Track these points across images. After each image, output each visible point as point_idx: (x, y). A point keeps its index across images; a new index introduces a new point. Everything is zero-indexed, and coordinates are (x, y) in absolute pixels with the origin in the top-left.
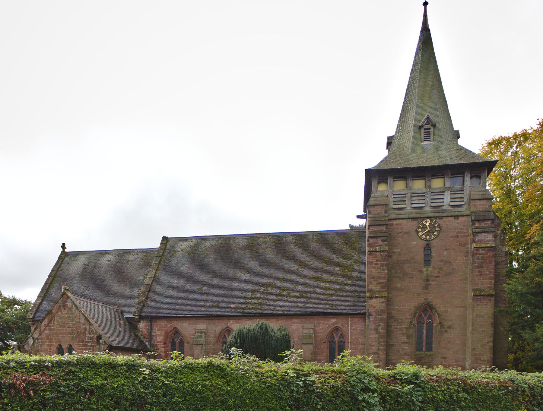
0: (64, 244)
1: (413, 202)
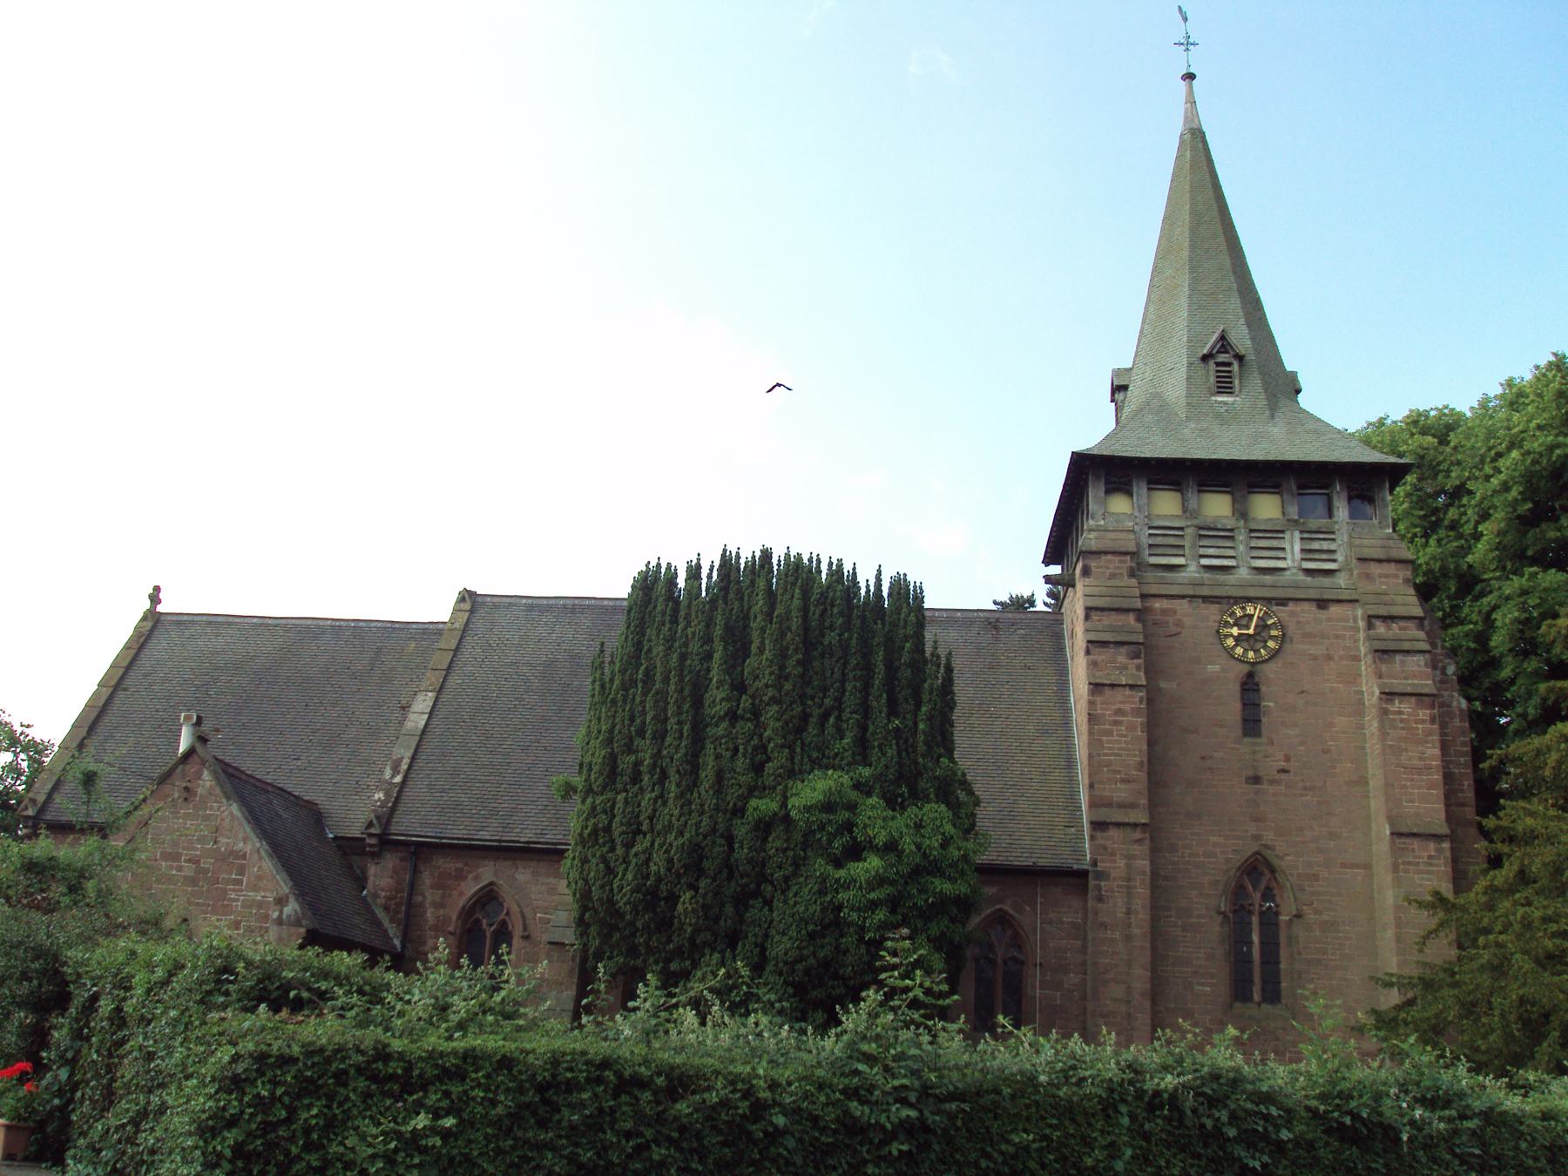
0: (157, 589)
1: (1202, 551)
